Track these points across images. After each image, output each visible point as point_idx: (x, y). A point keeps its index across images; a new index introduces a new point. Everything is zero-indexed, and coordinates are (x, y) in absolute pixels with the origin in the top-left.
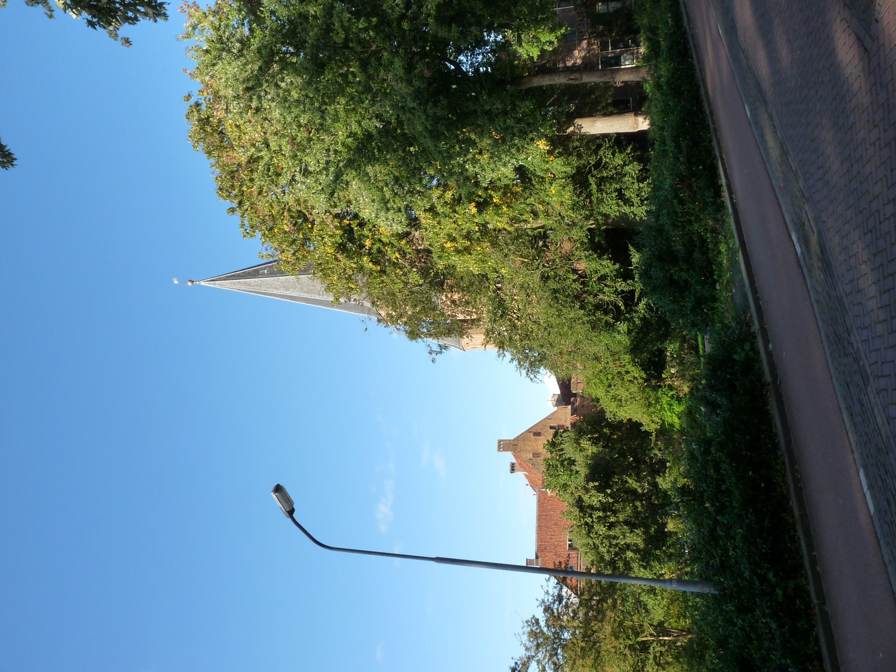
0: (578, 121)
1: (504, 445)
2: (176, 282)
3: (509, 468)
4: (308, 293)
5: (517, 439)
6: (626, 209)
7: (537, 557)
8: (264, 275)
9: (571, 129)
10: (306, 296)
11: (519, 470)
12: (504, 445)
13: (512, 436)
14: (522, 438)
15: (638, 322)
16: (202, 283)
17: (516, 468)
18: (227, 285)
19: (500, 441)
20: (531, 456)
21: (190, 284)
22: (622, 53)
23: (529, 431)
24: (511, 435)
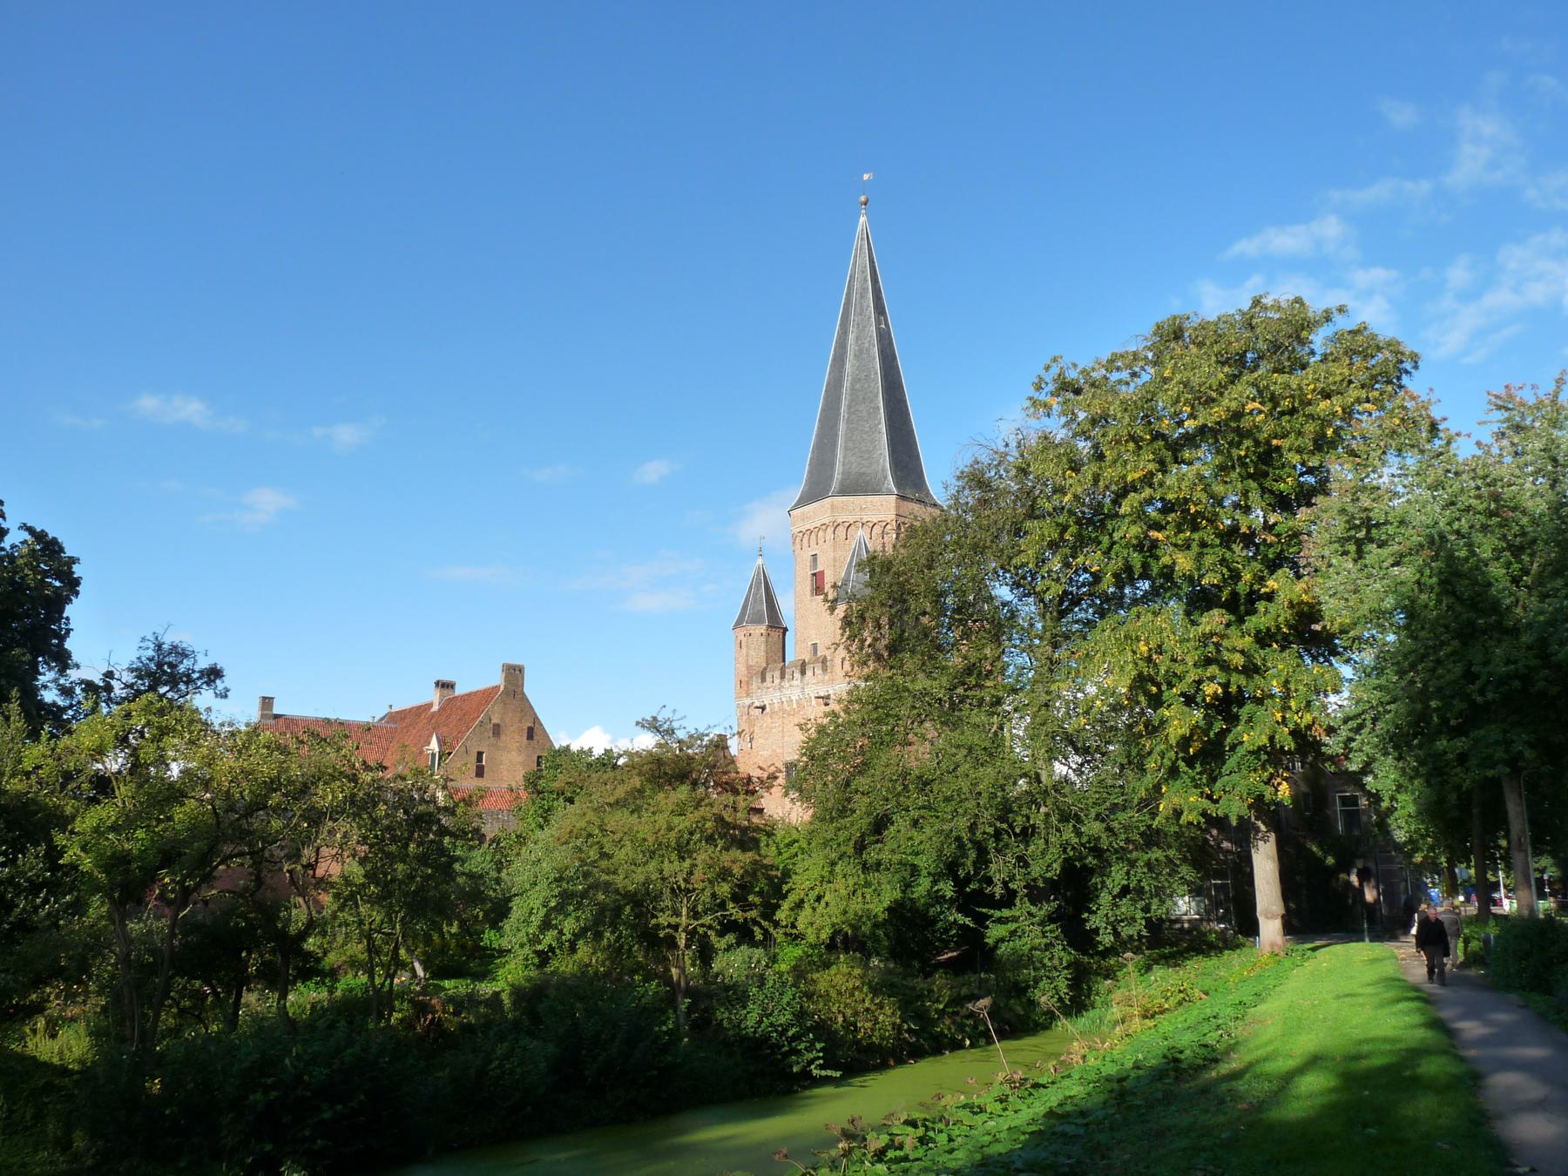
0: (1272, 837)
1: (514, 674)
2: (866, 177)
3: (446, 678)
4: (853, 388)
5: (524, 699)
6: (1105, 898)
7: (277, 717)
8: (878, 322)
9: (1263, 828)
10: (846, 384)
11: (442, 696)
12: (514, 674)
13: (529, 690)
14: (526, 708)
15: (932, 911)
16: (863, 219)
17: (445, 691)
18: (857, 261)
19: (521, 669)
20: (495, 721)
21: (863, 199)
22: (1210, 897)
23: (536, 719)
24: (530, 689)
